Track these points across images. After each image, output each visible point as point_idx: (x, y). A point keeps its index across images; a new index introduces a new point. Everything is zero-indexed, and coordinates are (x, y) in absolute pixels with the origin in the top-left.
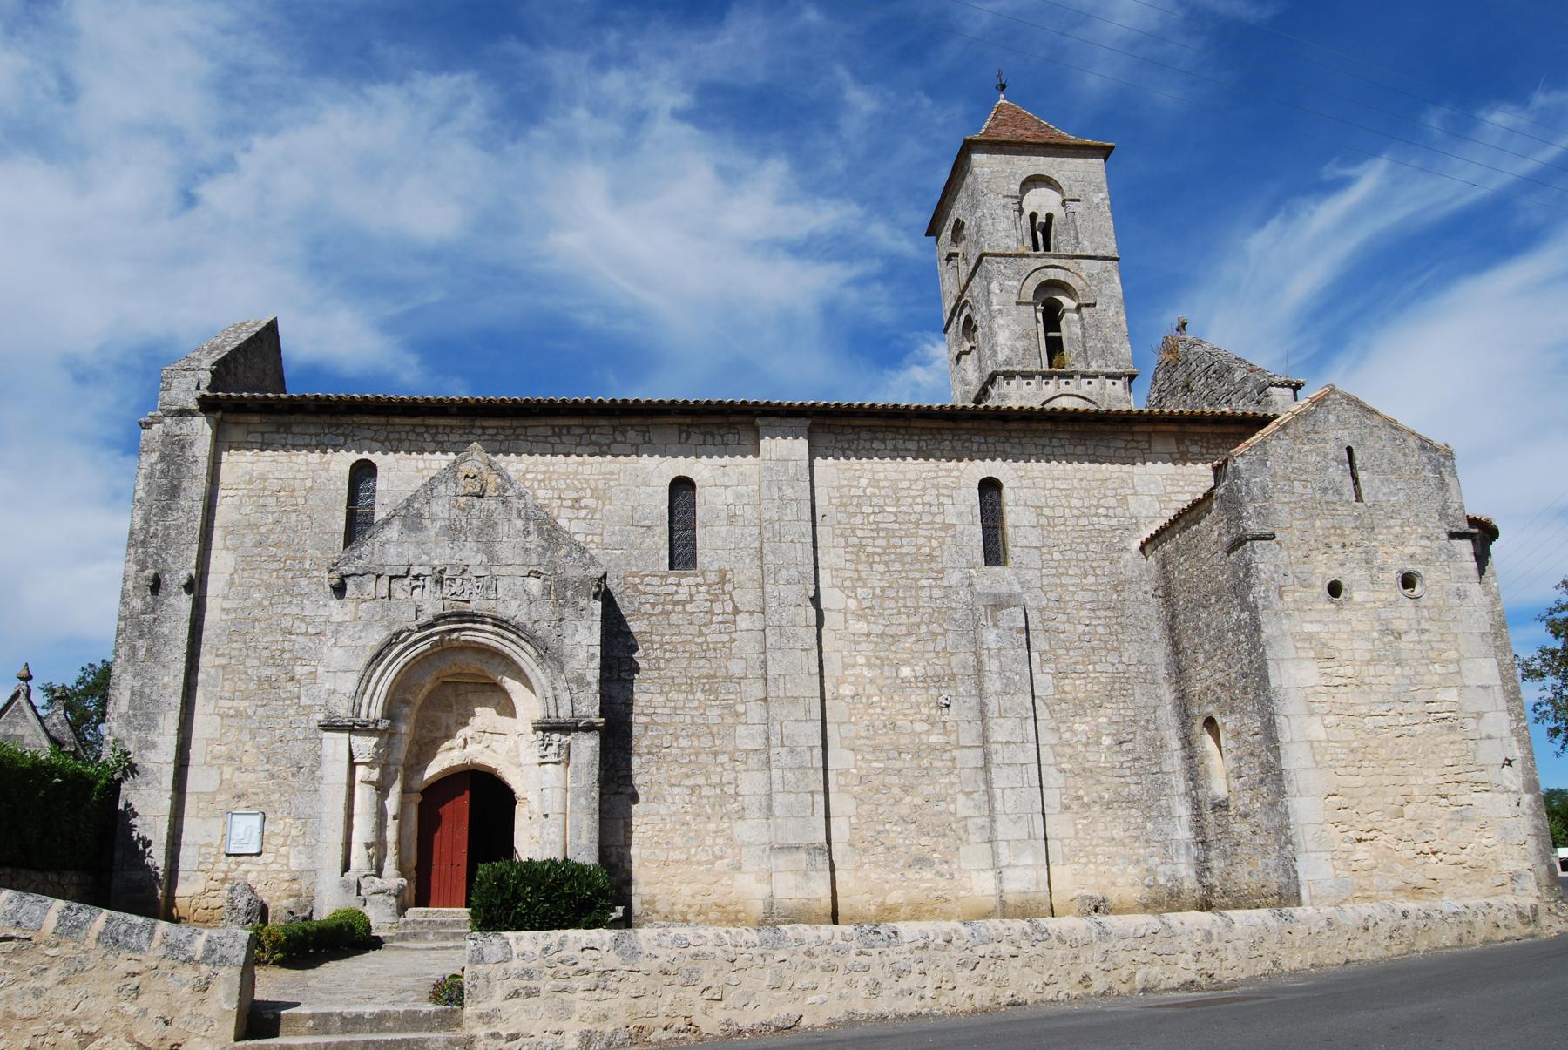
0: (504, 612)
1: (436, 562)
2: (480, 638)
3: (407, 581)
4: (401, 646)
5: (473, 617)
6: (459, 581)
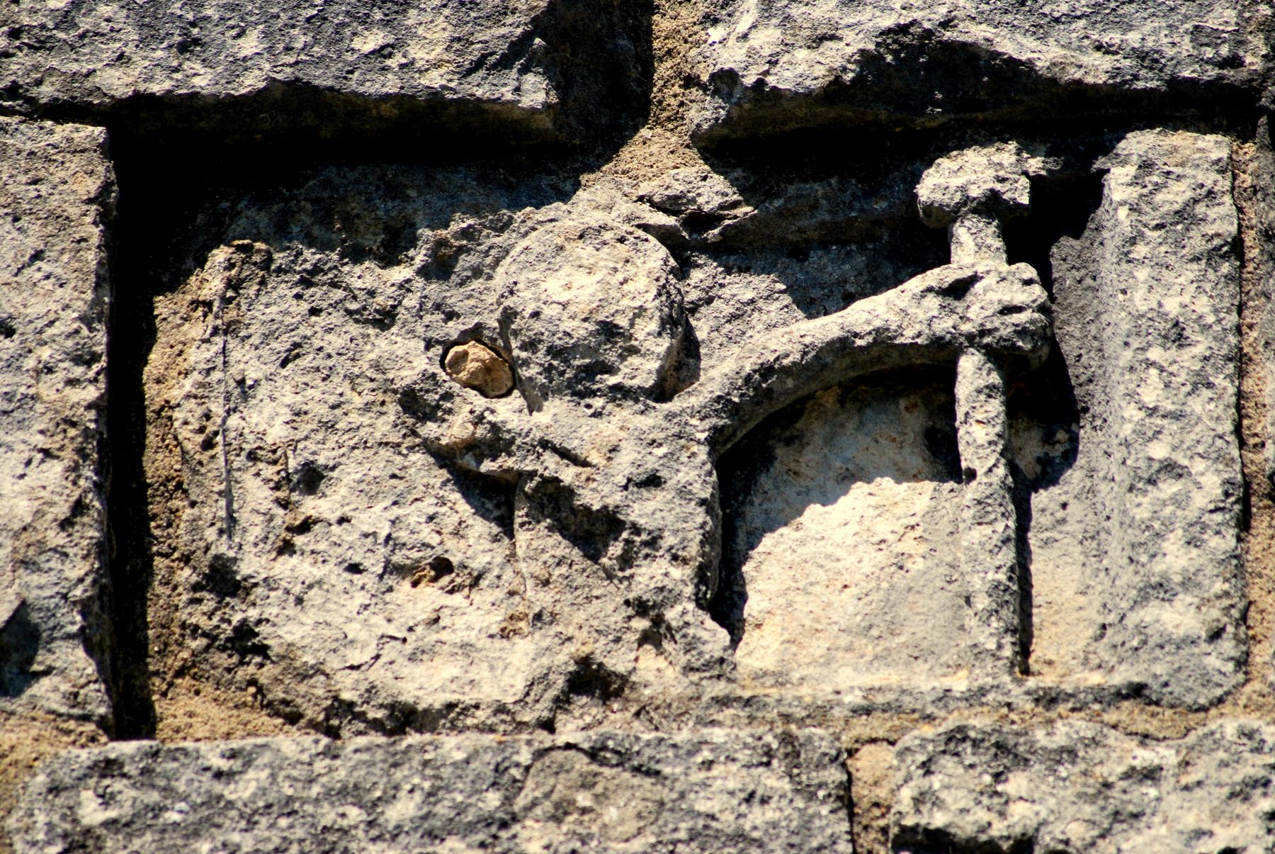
3: (578, 262)
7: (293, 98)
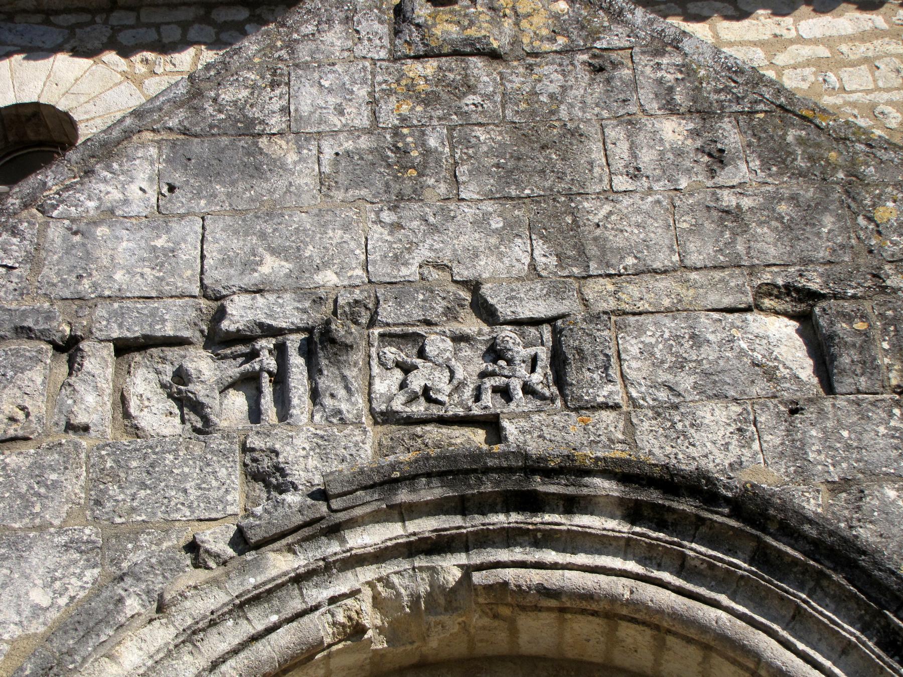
0: (654, 446)
1: (329, 278)
2: (571, 572)
4: (162, 634)
5: (527, 488)
6: (438, 344)
7: (145, 337)
